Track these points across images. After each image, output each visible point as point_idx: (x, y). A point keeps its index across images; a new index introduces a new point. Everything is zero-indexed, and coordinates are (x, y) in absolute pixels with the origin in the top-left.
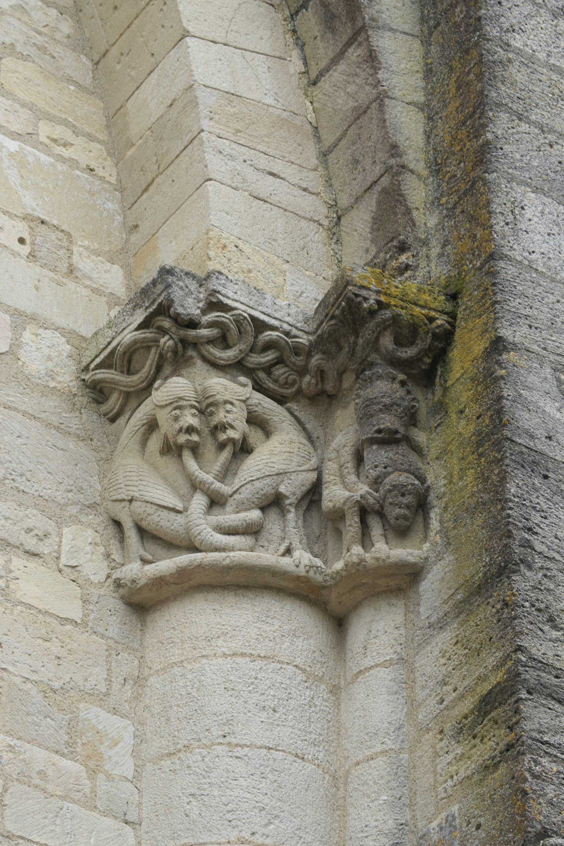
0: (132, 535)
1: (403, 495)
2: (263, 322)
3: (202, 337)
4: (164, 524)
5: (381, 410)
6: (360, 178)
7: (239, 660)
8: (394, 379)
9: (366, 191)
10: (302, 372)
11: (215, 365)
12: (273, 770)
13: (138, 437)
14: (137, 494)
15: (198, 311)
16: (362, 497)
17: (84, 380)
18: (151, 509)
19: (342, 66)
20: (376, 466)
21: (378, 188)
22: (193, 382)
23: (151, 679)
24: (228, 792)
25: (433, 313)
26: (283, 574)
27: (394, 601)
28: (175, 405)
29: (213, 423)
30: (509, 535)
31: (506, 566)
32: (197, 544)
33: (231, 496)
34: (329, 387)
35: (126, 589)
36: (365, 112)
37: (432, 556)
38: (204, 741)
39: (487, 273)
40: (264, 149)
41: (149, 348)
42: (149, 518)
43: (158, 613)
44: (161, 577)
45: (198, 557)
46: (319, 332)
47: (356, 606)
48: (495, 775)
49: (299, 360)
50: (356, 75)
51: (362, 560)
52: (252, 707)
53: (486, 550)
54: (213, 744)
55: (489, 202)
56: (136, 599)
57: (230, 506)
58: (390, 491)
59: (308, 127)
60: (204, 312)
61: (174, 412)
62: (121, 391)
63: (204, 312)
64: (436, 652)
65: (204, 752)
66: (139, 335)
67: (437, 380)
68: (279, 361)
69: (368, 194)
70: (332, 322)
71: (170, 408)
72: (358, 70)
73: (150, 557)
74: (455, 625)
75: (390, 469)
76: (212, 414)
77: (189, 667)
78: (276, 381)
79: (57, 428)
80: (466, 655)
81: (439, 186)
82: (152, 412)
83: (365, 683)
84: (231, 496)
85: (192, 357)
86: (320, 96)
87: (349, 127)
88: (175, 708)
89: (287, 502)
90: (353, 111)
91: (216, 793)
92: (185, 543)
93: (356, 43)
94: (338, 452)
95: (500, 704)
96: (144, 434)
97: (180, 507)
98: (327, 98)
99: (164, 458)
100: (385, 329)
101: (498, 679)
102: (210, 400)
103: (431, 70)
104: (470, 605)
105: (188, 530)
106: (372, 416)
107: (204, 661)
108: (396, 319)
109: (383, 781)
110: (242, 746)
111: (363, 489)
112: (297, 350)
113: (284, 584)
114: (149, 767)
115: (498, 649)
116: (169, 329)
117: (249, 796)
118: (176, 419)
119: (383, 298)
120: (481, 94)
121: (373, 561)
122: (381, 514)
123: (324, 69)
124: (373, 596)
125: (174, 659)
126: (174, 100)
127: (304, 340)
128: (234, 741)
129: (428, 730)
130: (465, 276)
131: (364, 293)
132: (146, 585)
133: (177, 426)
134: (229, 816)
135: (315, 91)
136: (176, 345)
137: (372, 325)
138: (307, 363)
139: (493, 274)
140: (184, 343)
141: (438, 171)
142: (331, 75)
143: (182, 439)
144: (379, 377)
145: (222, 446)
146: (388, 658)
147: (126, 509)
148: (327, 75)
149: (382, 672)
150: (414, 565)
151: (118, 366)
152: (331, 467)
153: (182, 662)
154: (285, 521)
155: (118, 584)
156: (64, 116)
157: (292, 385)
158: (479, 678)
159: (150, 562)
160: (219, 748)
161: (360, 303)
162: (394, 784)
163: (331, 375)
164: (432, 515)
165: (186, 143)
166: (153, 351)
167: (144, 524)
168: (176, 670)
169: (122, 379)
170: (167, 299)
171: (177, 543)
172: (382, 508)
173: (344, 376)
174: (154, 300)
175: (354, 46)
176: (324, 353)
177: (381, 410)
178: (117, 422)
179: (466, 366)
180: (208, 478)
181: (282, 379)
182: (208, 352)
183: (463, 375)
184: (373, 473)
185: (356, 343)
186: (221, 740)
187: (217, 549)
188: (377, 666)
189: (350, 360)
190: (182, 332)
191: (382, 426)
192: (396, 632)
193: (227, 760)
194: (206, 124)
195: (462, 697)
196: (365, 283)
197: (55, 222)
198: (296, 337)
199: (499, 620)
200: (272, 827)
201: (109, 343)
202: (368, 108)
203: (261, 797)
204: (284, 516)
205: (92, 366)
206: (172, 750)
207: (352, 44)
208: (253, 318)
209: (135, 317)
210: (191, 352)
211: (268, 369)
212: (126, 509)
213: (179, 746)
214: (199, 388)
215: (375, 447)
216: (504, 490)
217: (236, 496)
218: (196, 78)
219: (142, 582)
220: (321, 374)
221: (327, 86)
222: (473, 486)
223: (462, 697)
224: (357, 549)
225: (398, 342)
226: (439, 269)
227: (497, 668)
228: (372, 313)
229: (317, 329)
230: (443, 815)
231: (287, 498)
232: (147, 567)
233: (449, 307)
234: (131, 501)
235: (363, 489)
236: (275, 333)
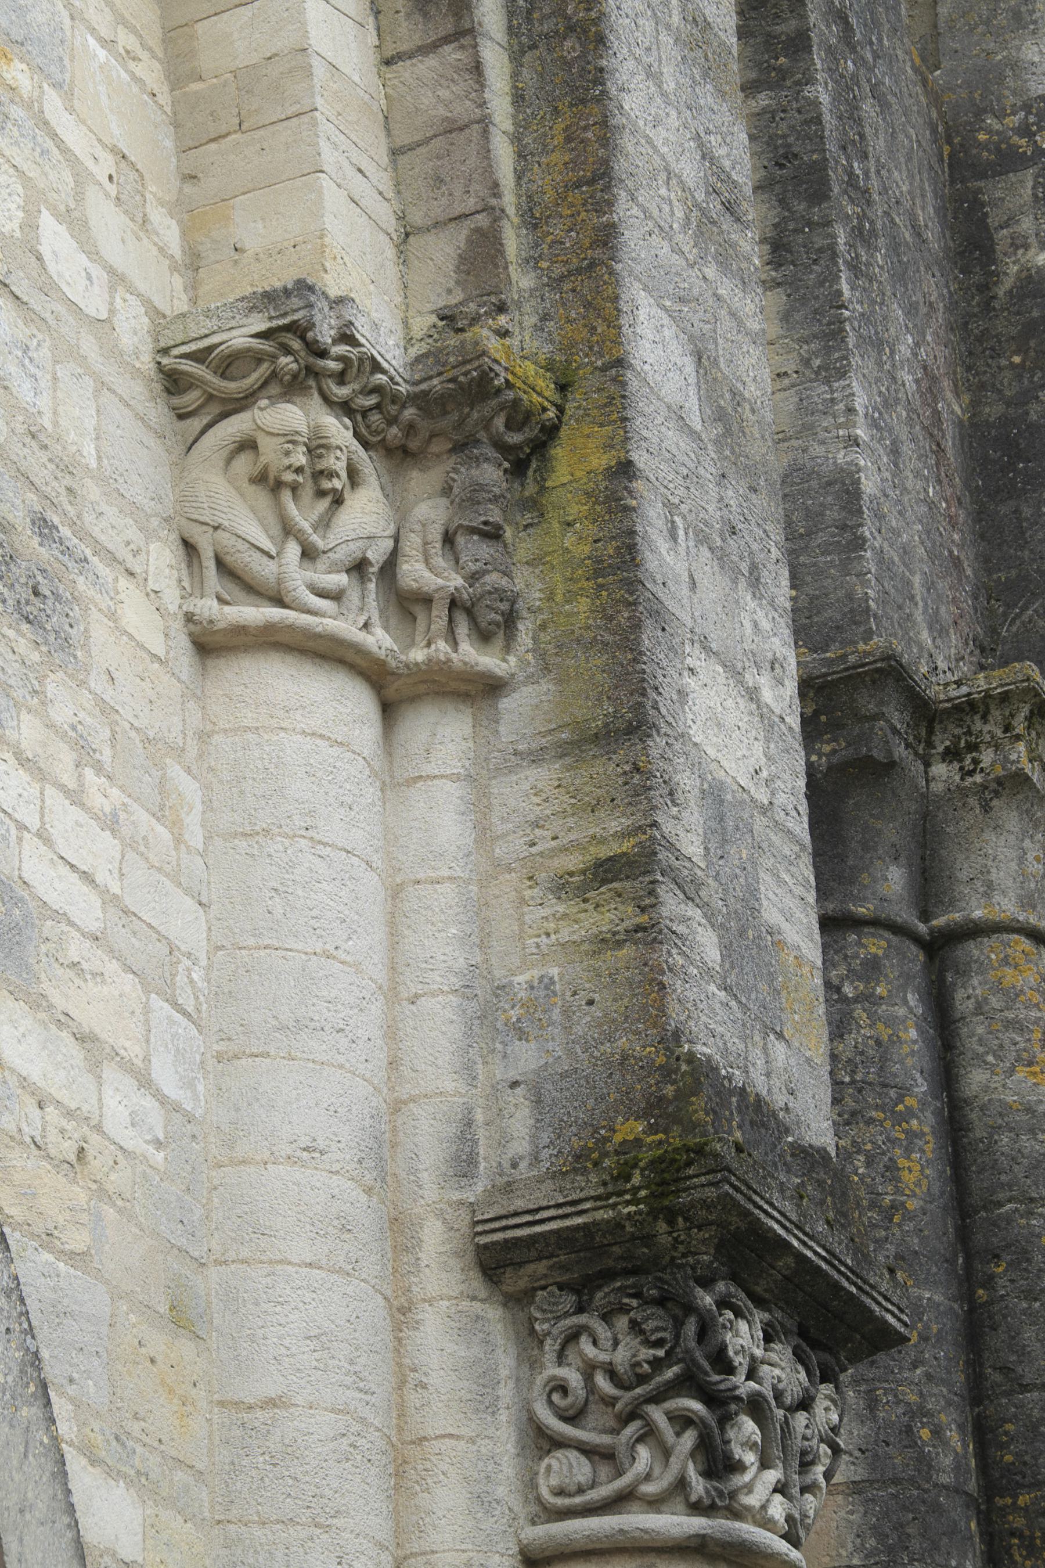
0: (210, 565)
1: (501, 600)
2: (378, 363)
3: (328, 370)
4: (255, 567)
5: (490, 500)
6: (444, 201)
7: (319, 741)
8: (500, 465)
9: (451, 220)
10: (392, 421)
11: (326, 399)
12: (351, 878)
13: (225, 453)
14: (226, 523)
15: (330, 341)
16: (456, 589)
17: (159, 363)
18: (241, 546)
19: (431, 61)
20: (477, 560)
21: (469, 224)
22: (307, 415)
23: (216, 737)
24: (313, 896)
25: (546, 403)
26: (358, 649)
27: (462, 707)
28: (289, 438)
29: (319, 467)
30: (644, 694)
31: (638, 727)
32: (286, 600)
33: (324, 552)
34: (413, 445)
35: (199, 627)
36: (461, 129)
37: (521, 676)
38: (286, 829)
39: (614, 380)
40: (355, 139)
41: (259, 361)
42: (238, 555)
43: (222, 661)
44: (244, 627)
45: (290, 616)
46: (424, 386)
47: (414, 699)
48: (620, 954)
49: (393, 409)
50: (453, 81)
51: (449, 660)
52: (332, 800)
53: (609, 698)
54: (295, 836)
55: (617, 298)
56: (203, 639)
57: (322, 563)
58: (490, 593)
59: (381, 116)
60: (335, 342)
61: (286, 446)
62: (205, 391)
63: (335, 342)
64: (526, 786)
65: (287, 842)
66: (256, 343)
67: (530, 473)
68: (378, 407)
69: (453, 224)
70: (451, 386)
71: (282, 440)
72: (456, 76)
73: (227, 597)
74: (557, 766)
75: (489, 567)
76: (320, 456)
77: (266, 737)
78: (368, 427)
79: (142, 419)
80: (573, 805)
81: (537, 245)
82: (251, 433)
83: (426, 792)
84: (324, 552)
85: (310, 387)
86: (396, 82)
87: (435, 136)
88: (250, 782)
89: (372, 570)
90: (443, 121)
91: (300, 892)
92: (271, 593)
93: (456, 44)
94: (424, 525)
95: (628, 877)
96: (232, 452)
97: (273, 553)
98: (405, 89)
99: (254, 487)
100: (502, 410)
101: (624, 849)
102: (323, 441)
103: (522, 97)
104: (582, 751)
105: (279, 581)
106: (479, 503)
107: (282, 734)
108: (516, 402)
109: (450, 912)
110: (325, 844)
111: (457, 581)
112: (395, 398)
113: (359, 661)
114: (218, 842)
115: (624, 814)
116: (297, 352)
117: (331, 903)
118: (287, 453)
119: (510, 377)
120: (606, 162)
121: (460, 664)
122: (469, 612)
123: (405, 53)
124: (437, 693)
125: (247, 723)
126: (276, 55)
127: (403, 388)
128: (317, 837)
129: (510, 870)
130: (577, 368)
131: (496, 367)
132: (225, 629)
133: (287, 462)
134: (312, 922)
135: (389, 73)
136: (300, 370)
137: (494, 403)
138: (400, 412)
139: (623, 384)
140: (311, 371)
141: (535, 226)
142: (415, 65)
143: (289, 477)
144: (487, 460)
145: (321, 493)
146: (455, 771)
147: (208, 535)
148: (408, 62)
149: (449, 786)
150: (501, 678)
151: (213, 364)
152: (412, 543)
153: (257, 728)
154: (363, 590)
155: (189, 618)
156: (134, 22)
157: (379, 433)
158: (594, 837)
159: (227, 603)
160: (303, 842)
161: (492, 379)
162: (463, 918)
163: (424, 434)
164: (521, 626)
165: (289, 114)
166: (266, 365)
167: (228, 559)
168: (250, 736)
169: (214, 380)
170: (308, 321)
171: (263, 591)
172: (473, 605)
173: (434, 440)
174: (285, 314)
175: (453, 45)
176: (420, 409)
177: (490, 500)
178: (189, 421)
179: (578, 474)
180: (306, 526)
181: (374, 427)
182: (329, 388)
183: (571, 482)
184: (473, 567)
185: (468, 415)
186: (303, 832)
187: (309, 612)
188: (442, 776)
189: (454, 429)
190: (311, 360)
191: (491, 519)
192: (463, 743)
193: (311, 857)
194: (319, 102)
195: (564, 850)
196: (498, 357)
197: (133, 159)
198: (397, 384)
199: (626, 784)
200: (351, 943)
201: (206, 336)
202: (467, 126)
203: (341, 908)
204: (363, 583)
205: (176, 352)
206: (248, 829)
207: (451, 42)
208: (373, 359)
209: (250, 320)
210: (312, 382)
211: (365, 413)
212: (208, 535)
213: (257, 828)
214: (312, 423)
215: (476, 537)
216: (638, 641)
217: (330, 554)
218: (311, 42)
219: (221, 625)
220: (410, 428)
221: (407, 75)
222: (588, 618)
223: (564, 850)
224: (442, 646)
225: (508, 426)
226: (536, 344)
227: (624, 835)
228: (498, 391)
229: (420, 382)
230: (536, 973)
231: (371, 564)
232: (227, 609)
233: (556, 398)
234: (216, 528)
235: (457, 581)
236: (385, 378)
